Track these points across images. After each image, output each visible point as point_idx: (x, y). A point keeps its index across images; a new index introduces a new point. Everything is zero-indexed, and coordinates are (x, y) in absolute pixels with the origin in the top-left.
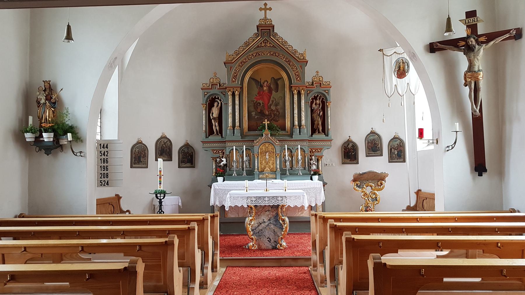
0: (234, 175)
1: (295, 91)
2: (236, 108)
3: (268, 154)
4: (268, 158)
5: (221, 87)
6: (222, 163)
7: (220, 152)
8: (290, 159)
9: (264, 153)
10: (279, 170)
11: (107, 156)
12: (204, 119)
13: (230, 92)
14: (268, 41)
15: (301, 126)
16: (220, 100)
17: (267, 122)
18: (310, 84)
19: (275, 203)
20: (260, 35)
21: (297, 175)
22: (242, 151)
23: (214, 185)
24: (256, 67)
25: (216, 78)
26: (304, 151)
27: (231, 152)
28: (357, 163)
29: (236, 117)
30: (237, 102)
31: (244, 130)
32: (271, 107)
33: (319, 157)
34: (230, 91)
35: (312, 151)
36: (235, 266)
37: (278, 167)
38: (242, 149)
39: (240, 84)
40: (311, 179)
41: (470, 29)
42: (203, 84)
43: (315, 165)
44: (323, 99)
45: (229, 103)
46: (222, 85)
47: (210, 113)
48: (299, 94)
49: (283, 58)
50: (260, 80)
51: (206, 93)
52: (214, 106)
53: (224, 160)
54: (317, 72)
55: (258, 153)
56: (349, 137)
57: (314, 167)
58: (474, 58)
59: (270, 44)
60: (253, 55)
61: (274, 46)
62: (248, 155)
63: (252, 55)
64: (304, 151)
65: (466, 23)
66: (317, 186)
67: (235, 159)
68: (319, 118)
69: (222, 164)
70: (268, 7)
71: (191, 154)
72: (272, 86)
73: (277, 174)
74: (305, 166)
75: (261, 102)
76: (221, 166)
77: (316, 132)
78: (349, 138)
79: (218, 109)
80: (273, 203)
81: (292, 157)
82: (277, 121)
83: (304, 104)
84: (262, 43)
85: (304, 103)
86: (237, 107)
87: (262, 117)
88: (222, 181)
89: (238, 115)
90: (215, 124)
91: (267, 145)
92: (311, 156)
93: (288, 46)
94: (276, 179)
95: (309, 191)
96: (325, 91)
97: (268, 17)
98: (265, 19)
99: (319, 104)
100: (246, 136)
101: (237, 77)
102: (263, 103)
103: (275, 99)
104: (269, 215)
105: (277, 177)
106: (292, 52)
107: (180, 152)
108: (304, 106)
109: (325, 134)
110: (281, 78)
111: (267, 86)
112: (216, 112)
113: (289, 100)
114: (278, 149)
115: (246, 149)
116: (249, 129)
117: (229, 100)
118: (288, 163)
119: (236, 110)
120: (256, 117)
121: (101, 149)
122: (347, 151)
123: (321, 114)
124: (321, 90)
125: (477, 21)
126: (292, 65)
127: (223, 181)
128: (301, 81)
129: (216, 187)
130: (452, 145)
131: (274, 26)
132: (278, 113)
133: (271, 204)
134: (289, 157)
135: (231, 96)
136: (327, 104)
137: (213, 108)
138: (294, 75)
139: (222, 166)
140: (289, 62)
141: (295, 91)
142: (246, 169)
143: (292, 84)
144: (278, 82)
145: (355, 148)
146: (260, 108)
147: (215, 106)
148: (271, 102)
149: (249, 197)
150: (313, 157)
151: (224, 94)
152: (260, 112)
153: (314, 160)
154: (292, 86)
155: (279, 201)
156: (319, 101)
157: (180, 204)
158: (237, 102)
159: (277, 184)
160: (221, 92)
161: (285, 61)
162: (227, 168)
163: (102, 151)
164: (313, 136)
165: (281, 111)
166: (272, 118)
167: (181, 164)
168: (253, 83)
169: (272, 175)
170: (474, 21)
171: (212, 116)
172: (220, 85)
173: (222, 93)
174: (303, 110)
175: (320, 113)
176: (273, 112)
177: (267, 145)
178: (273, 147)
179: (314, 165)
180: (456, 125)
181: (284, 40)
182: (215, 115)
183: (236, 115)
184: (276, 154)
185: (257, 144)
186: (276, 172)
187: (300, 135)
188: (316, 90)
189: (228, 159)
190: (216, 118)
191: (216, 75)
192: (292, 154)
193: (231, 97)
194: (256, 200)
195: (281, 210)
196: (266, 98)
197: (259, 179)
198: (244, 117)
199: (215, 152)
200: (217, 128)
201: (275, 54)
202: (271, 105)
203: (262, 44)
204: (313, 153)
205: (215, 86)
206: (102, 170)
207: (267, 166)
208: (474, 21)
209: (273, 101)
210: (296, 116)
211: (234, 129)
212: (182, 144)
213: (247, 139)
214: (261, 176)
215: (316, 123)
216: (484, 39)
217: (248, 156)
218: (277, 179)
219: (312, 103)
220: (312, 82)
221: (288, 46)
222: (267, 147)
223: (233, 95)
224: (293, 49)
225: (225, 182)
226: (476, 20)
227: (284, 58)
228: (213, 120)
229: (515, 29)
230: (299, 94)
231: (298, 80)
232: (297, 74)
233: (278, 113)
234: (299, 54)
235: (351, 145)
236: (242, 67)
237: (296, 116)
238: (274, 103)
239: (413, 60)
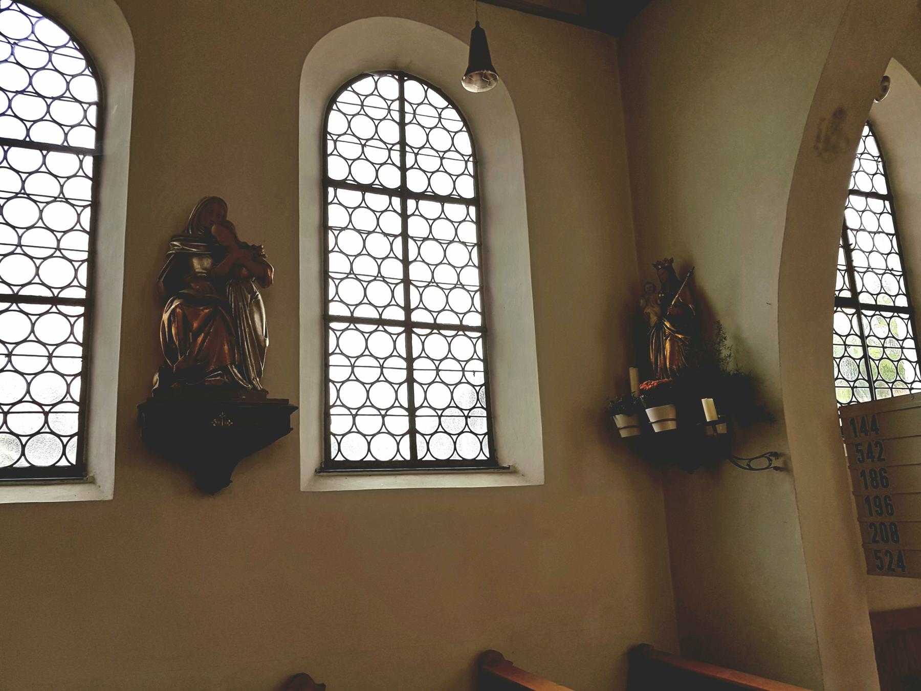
11: (880, 459)
36: (470, 130)
121: (856, 436)
163: (861, 445)
206: (874, 513)
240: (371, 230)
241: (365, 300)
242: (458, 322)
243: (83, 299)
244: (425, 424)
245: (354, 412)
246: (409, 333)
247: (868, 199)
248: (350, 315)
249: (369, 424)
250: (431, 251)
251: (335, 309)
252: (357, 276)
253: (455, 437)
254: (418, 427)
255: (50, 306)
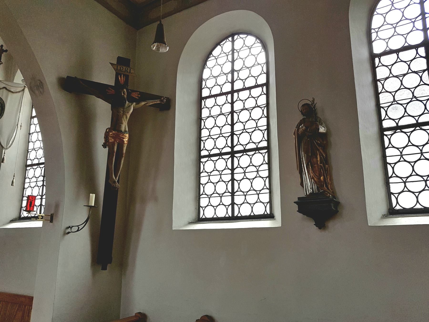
41: (124, 76)
58: (123, 115)
65: (117, 70)
88: (112, 62)
125: (130, 73)
130: (78, 226)
170: (126, 71)
180: (92, 197)
208: (127, 71)
216: (136, 95)
226: (128, 71)
228: (45, 181)
229: (165, 97)
239: (37, 92)
240: (406, 73)
241: (406, 114)
242: (415, 122)
243: (266, 147)
244: (238, 200)
245: (209, 196)
246: (232, 157)
247: (231, 55)
248: (396, 125)
249: (252, 199)
250: (244, 116)
251: (386, 124)
252: (397, 102)
253: (252, 205)
254: (235, 201)
255: (208, 158)
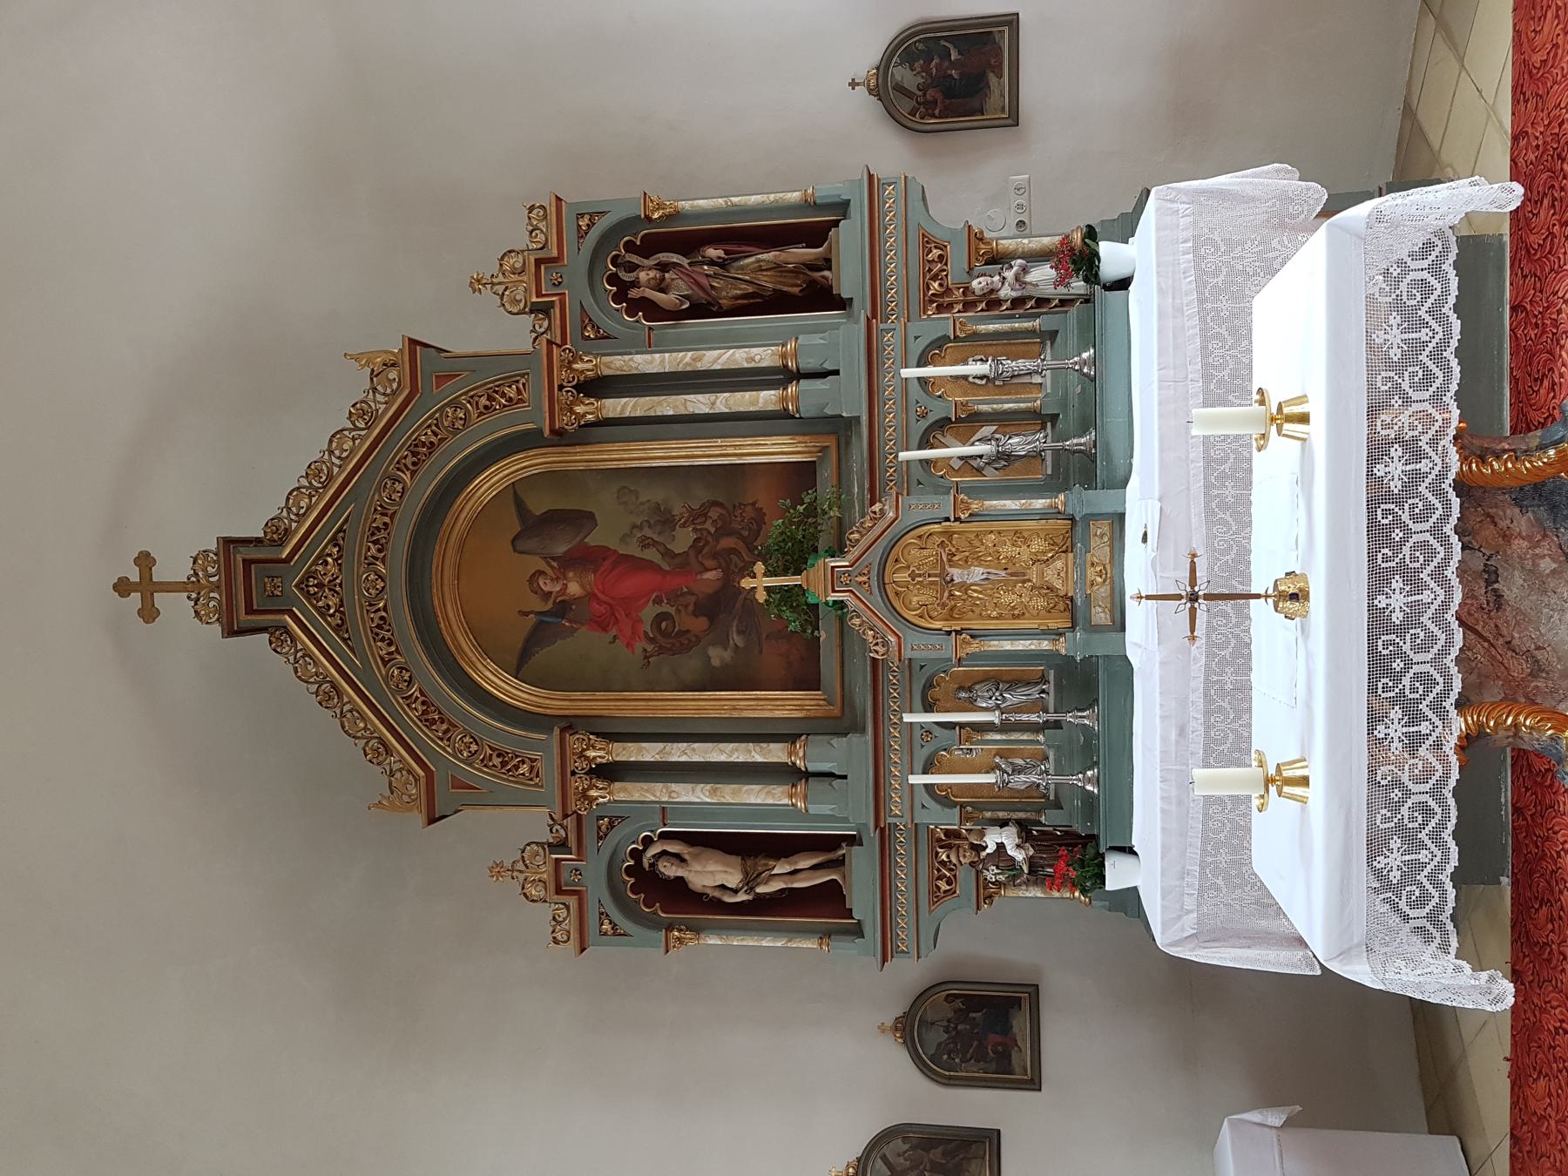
0: (1089, 787)
1: (579, 409)
2: (684, 759)
3: (957, 574)
4: (982, 570)
5: (572, 843)
6: (1011, 851)
7: (944, 857)
8: (987, 430)
9: (951, 599)
10: (1062, 497)
12: (750, 942)
13: (593, 793)
14: (310, 575)
15: (786, 366)
16: (648, 842)
17: (759, 575)
18: (546, 324)
19: (1445, 518)
20: (278, 617)
21: (1094, 379)
22: (937, 731)
23: (1173, 944)
24: (454, 638)
25: (520, 866)
26: (941, 342)
27: (946, 797)
28: (1011, 22)
29: (733, 759)
30: (649, 752)
31: (812, 714)
32: (677, 552)
33: (977, 250)
34: (584, 795)
35: (942, 295)
37: (1039, 503)
38: (927, 730)
39: (543, 737)
40: (1123, 284)
42: (556, 941)
43: (1025, 270)
44: (630, 247)
45: (653, 798)
46: (562, 833)
47: (720, 901)
48: (597, 387)
49: (399, 487)
50: (526, 614)
51: (607, 926)
52: (682, 878)
53: (992, 839)
54: (477, 284)
55: (949, 633)
56: (853, 84)
57: (1043, 276)
59: (326, 563)
60: (387, 658)
61: (334, 538)
62: (965, 692)
63: (385, 663)
64: (940, 347)
66: (1183, 235)
67: (989, 779)
68: (742, 268)
69: (1019, 856)
70: (134, 577)
71: (959, 1004)
72: (561, 549)
73: (1085, 511)
74: (1032, 333)
75: (649, 612)
76: (1031, 861)
77: (826, 278)
78: (861, 90)
79: (696, 857)
80: (1436, 531)
81: (977, 419)
82: (760, 520)
83: (657, 356)
84: (320, 604)
85: (648, 357)
86: (679, 753)
87: (738, 606)
89: (721, 745)
90: (779, 877)
91: (903, 577)
92: (968, 306)
93: (334, 460)
94: (1121, 518)
95: (1222, 277)
96: (582, 235)
97: (182, 572)
98: (191, 586)
99: (664, 267)
100: (846, 700)
101: (508, 749)
102: (655, 602)
103: (634, 527)
104: (1533, 573)
105: (1110, 510)
106: (363, 433)
107: (950, 1078)
108: (667, 355)
109: (836, 224)
110: (515, 493)
111: (557, 579)
112: (712, 867)
113: (633, 446)
114: (923, 506)
115: (928, 708)
116: (807, 679)
117: (636, 797)
118: (1017, 444)
119: (696, 759)
120: (737, 639)
122: (939, 97)
123: (720, 253)
124: (577, 260)
126: (435, 434)
127: (1135, 854)
128: (522, 376)
129: (1183, 930)
131: (228, 543)
132: (714, 513)
133: (1446, 560)
134: (978, 436)
135: (617, 785)
136: (656, 216)
137: (690, 886)
138: (488, 419)
139: (1031, 852)
140: (419, 452)
141: (579, 409)
142: (1051, 709)
143: (540, 431)
144: (538, 514)
145: (920, 46)
146: (683, 613)
147: (680, 873)
148: (652, 555)
149: (1372, 771)
150: (978, 284)
151: (611, 826)
152: (712, 620)
153: (997, 278)
154: (553, 431)
155: (1417, 477)
156: (641, 267)
157: (1275, 1118)
158: (649, 752)
159: (1163, 507)
160: (600, 838)
161: (413, 473)
162: (1043, 819)
164: (845, 295)
165: (700, 495)
166: (741, 546)
167: (1017, 1069)
168: (544, 656)
169: (1094, 542)
171: (735, 891)
172: (561, 845)
173: (606, 835)
174: (687, 359)
175: (712, 263)
176: (707, 543)
177: (903, 577)
178: (909, 539)
179: (1029, 278)
181: (304, 482)
182: (729, 878)
183: (723, 758)
184: (957, 519)
185: (892, 639)
186: (1072, 519)
187: (836, 373)
188: (576, 290)
189: (988, 814)
190: (746, 873)
191: (508, 864)
192: (958, 420)
193: (621, 790)
194: (1400, 699)
195: (1498, 457)
196: (630, 584)
197: (1123, 629)
198: (735, 714)
199: (944, 886)
200: (805, 863)
201: (378, 528)
202: (668, 554)
203: (329, 607)
204: (948, 291)
205: (565, 875)
207: (1033, 573)
209: (646, 543)
210: (724, 402)
211: (807, 775)
212: (896, 1060)
213: (864, 699)
214: (1100, 616)
215: (767, 282)
217: (970, 690)
218: (1120, 510)
219: (653, 311)
220: (531, 312)
221: (334, 460)
222: (913, 576)
223: (610, 772)
224: (350, 430)
225: (1136, 843)
227: (396, 480)
228: (760, 890)
230: (597, 387)
231: (519, 392)
232: (484, 401)
233: (714, 513)
234: (375, 390)
235: (905, 76)
236: (454, 720)
237: (724, 402)
238: (655, 537)
